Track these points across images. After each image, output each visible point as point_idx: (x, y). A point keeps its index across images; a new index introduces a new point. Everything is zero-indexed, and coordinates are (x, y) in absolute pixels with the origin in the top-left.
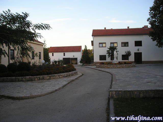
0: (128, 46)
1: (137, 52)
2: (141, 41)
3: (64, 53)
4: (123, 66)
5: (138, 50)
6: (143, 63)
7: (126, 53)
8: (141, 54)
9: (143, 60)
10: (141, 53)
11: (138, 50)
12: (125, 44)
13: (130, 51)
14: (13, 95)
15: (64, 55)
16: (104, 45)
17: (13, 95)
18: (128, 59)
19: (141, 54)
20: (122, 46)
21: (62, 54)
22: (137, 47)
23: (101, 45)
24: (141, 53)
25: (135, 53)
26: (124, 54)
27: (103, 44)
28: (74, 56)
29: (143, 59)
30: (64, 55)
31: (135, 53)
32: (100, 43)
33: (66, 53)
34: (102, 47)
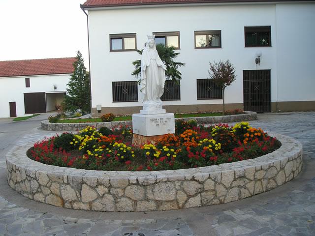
0: (220, 46)
1: (255, 67)
2: (269, 28)
3: (27, 77)
4: (209, 185)
5: (258, 61)
6: (277, 111)
7: (213, 69)
8: (265, 75)
9: (274, 98)
10: (268, 72)
11: (258, 61)
12: (214, 39)
13: (231, 62)
14: (155, 75)
15: (28, 85)
16: (129, 43)
17: (155, 75)
18: (220, 96)
19: (265, 75)
20: (111, 51)
21: (22, 80)
22: (255, 51)
23: (117, 44)
24: (268, 72)
25: (245, 72)
26: (207, 75)
27: (126, 40)
28: (55, 88)
29: (276, 96)
30: (28, 85)
31: (245, 72)
32: (113, 37)
33: (33, 80)
34: (123, 50)
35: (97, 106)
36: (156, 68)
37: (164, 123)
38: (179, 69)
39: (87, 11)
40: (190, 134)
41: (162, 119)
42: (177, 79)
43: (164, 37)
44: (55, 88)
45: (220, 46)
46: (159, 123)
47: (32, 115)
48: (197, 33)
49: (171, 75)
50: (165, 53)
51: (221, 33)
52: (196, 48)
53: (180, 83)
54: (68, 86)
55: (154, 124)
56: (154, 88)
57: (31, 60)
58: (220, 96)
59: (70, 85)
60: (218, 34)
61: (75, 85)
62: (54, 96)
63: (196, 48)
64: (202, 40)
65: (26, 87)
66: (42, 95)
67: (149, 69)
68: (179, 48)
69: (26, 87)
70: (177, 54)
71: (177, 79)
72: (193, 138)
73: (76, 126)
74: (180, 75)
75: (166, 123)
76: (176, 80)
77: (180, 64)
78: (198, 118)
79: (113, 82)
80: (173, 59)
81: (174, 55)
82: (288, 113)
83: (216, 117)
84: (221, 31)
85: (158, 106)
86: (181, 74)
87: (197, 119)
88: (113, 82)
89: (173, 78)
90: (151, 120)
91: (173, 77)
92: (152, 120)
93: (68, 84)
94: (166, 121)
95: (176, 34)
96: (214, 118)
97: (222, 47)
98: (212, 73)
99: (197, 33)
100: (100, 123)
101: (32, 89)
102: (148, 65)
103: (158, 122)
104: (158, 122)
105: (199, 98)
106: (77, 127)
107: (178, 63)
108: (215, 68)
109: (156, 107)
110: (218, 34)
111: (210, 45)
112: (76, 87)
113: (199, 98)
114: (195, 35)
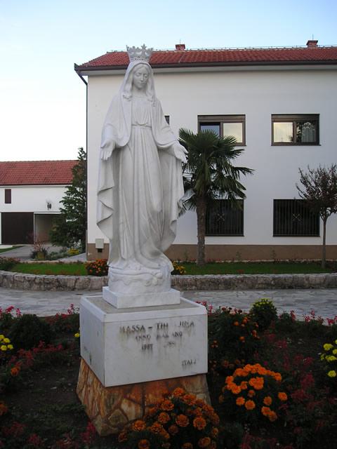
0: (316, 142)
3: (8, 188)
7: (305, 182)
15: (8, 200)
26: (293, 191)
28: (50, 206)
30: (8, 200)
33: (16, 192)
35: (96, 240)
36: (152, 154)
37: (171, 339)
38: (242, 179)
39: (86, 78)
40: (258, 384)
41: (165, 326)
42: (238, 198)
43: (218, 124)
44: (50, 206)
45: (316, 142)
46: (153, 340)
47: (11, 246)
48: (276, 118)
49: (227, 190)
50: (215, 149)
51: (318, 118)
52: (274, 144)
53: (242, 206)
54: (62, 204)
55: (133, 344)
56: (145, 220)
57: (16, 163)
58: (314, 232)
59: (65, 202)
60: (314, 119)
61: (74, 202)
62: (47, 218)
63: (274, 144)
64: (285, 131)
65: (6, 202)
66: (27, 217)
67: (127, 156)
68: (244, 144)
69: (6, 202)
70: (239, 151)
71: (238, 198)
72: (268, 400)
73: (37, 281)
74: (243, 191)
75: (177, 341)
76: (235, 201)
77: (245, 170)
78: (277, 276)
79: (275, 200)
80: (231, 160)
81: (232, 154)
82: (136, 155)
83: (312, 276)
84: (318, 115)
85: (155, 280)
86: (244, 189)
87: (274, 279)
88: (275, 200)
89: (230, 196)
90: (123, 330)
91: (230, 193)
92: (127, 332)
93: (62, 201)
94: (176, 335)
95: (240, 119)
96: (308, 279)
97: (320, 143)
98: (304, 188)
99: (276, 118)
100: (82, 278)
101: (13, 208)
102: (122, 144)
103: (147, 337)
104: (147, 337)
105: (277, 233)
106: (40, 283)
107: (241, 169)
108: (310, 179)
109: (149, 283)
110: (314, 119)
111: (297, 141)
112: (75, 205)
113: (277, 233)
114: (273, 122)
